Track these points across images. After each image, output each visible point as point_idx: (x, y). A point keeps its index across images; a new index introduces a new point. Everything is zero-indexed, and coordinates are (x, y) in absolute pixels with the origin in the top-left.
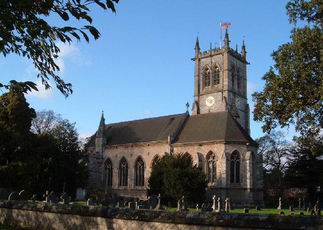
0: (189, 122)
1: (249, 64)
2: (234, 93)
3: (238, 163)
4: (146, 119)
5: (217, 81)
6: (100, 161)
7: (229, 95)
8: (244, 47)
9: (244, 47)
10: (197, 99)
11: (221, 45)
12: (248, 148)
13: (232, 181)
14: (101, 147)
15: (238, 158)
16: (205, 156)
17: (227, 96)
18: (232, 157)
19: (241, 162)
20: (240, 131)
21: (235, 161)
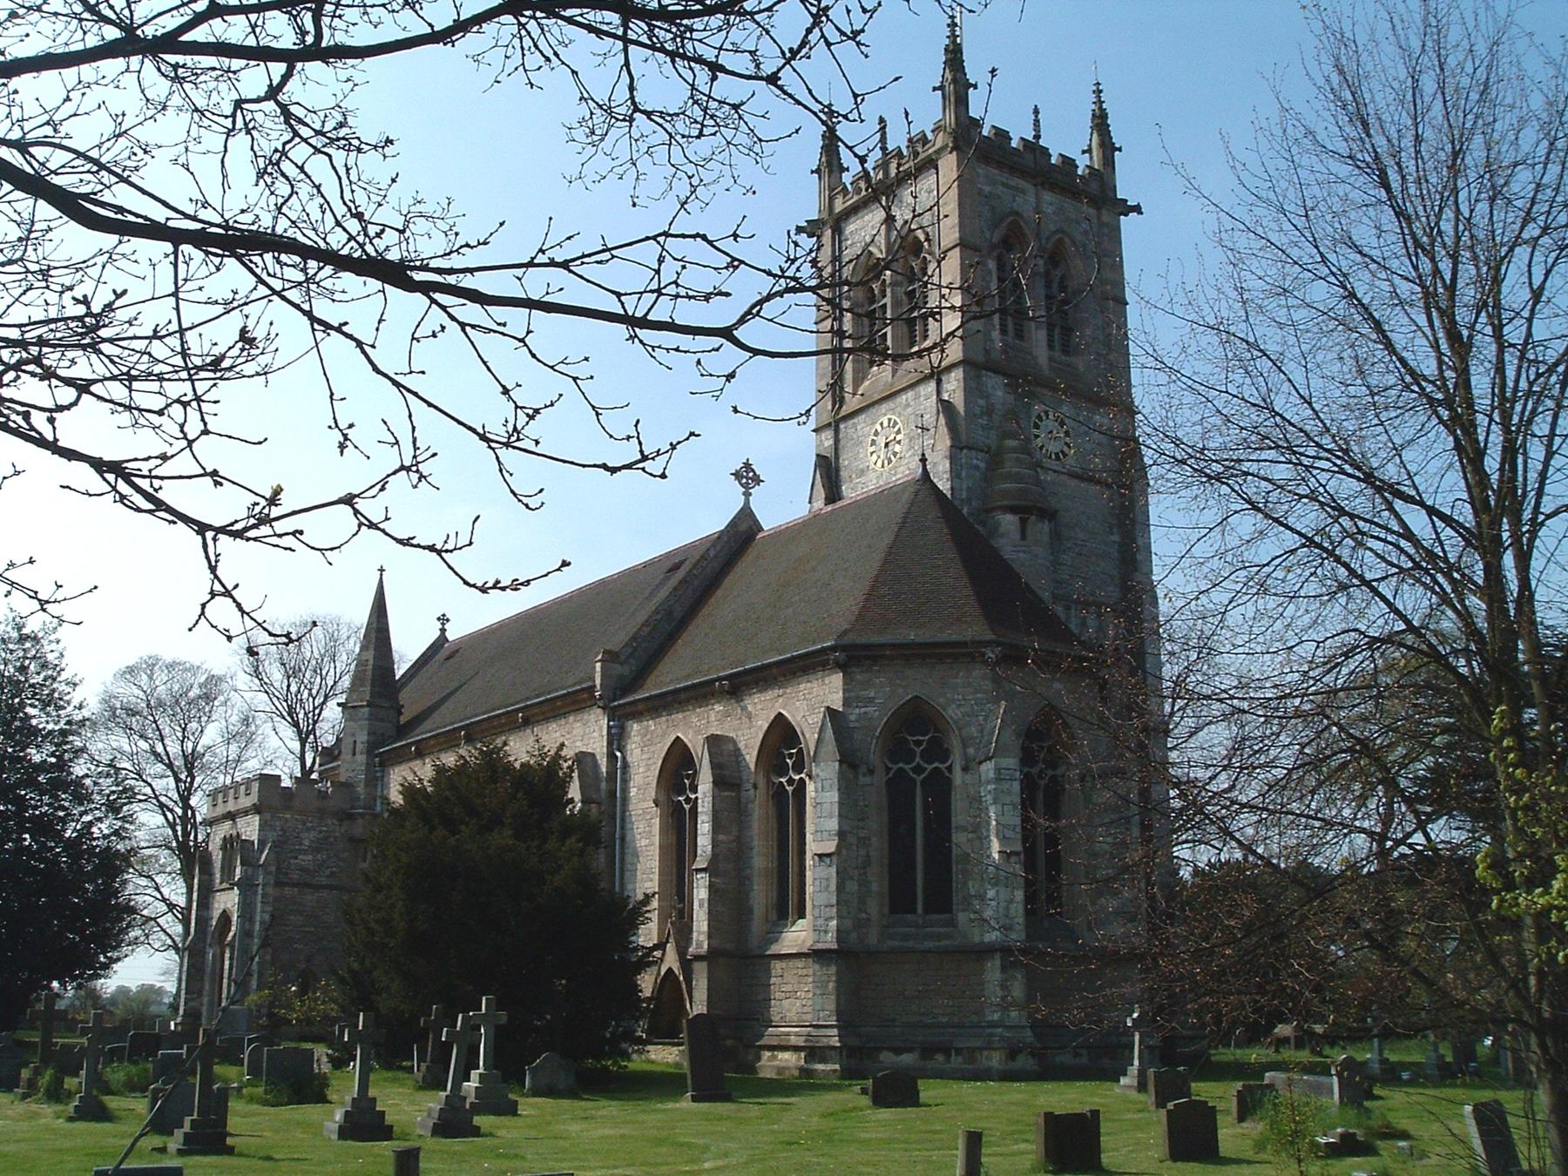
0: (751, 554)
1: (1137, 209)
2: (1024, 380)
3: (940, 787)
4: (603, 583)
5: (914, 318)
6: (358, 829)
7: (969, 391)
8: (1100, 121)
9: (1100, 121)
10: (827, 439)
11: (929, 113)
12: (997, 680)
13: (900, 901)
14: (361, 758)
15: (938, 751)
16: (751, 758)
17: (958, 400)
18: (896, 748)
19: (958, 777)
20: (879, 564)
21: (918, 770)
